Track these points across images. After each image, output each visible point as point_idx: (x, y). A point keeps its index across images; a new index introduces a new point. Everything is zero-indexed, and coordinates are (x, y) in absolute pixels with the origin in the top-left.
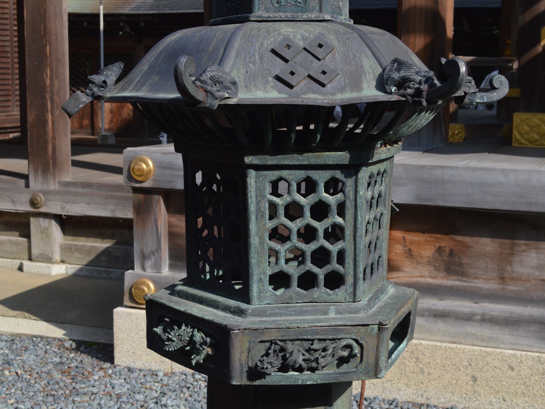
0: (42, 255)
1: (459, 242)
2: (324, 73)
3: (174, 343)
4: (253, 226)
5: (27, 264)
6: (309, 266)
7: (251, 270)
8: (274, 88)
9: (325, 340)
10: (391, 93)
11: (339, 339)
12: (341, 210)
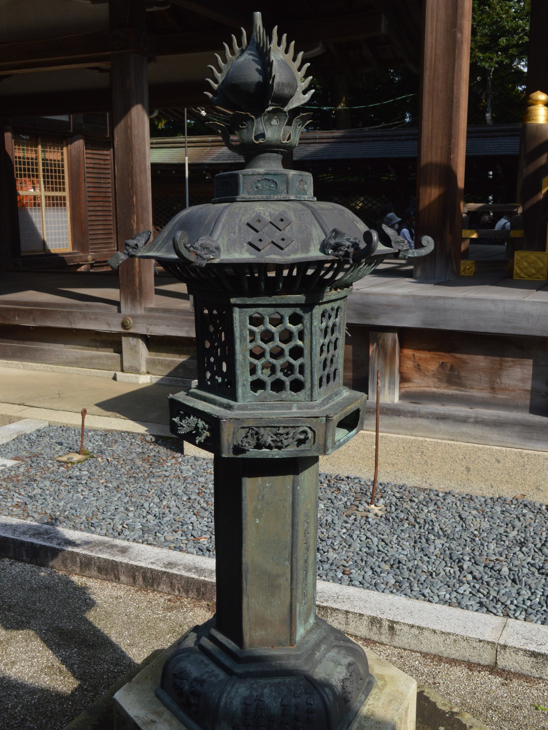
0: (132, 367)
1: (458, 358)
2: (283, 240)
4: (238, 347)
5: (119, 374)
6: (280, 375)
7: (237, 378)
8: (247, 251)
9: (288, 427)
10: (328, 254)
11: (298, 427)
12: (301, 336)
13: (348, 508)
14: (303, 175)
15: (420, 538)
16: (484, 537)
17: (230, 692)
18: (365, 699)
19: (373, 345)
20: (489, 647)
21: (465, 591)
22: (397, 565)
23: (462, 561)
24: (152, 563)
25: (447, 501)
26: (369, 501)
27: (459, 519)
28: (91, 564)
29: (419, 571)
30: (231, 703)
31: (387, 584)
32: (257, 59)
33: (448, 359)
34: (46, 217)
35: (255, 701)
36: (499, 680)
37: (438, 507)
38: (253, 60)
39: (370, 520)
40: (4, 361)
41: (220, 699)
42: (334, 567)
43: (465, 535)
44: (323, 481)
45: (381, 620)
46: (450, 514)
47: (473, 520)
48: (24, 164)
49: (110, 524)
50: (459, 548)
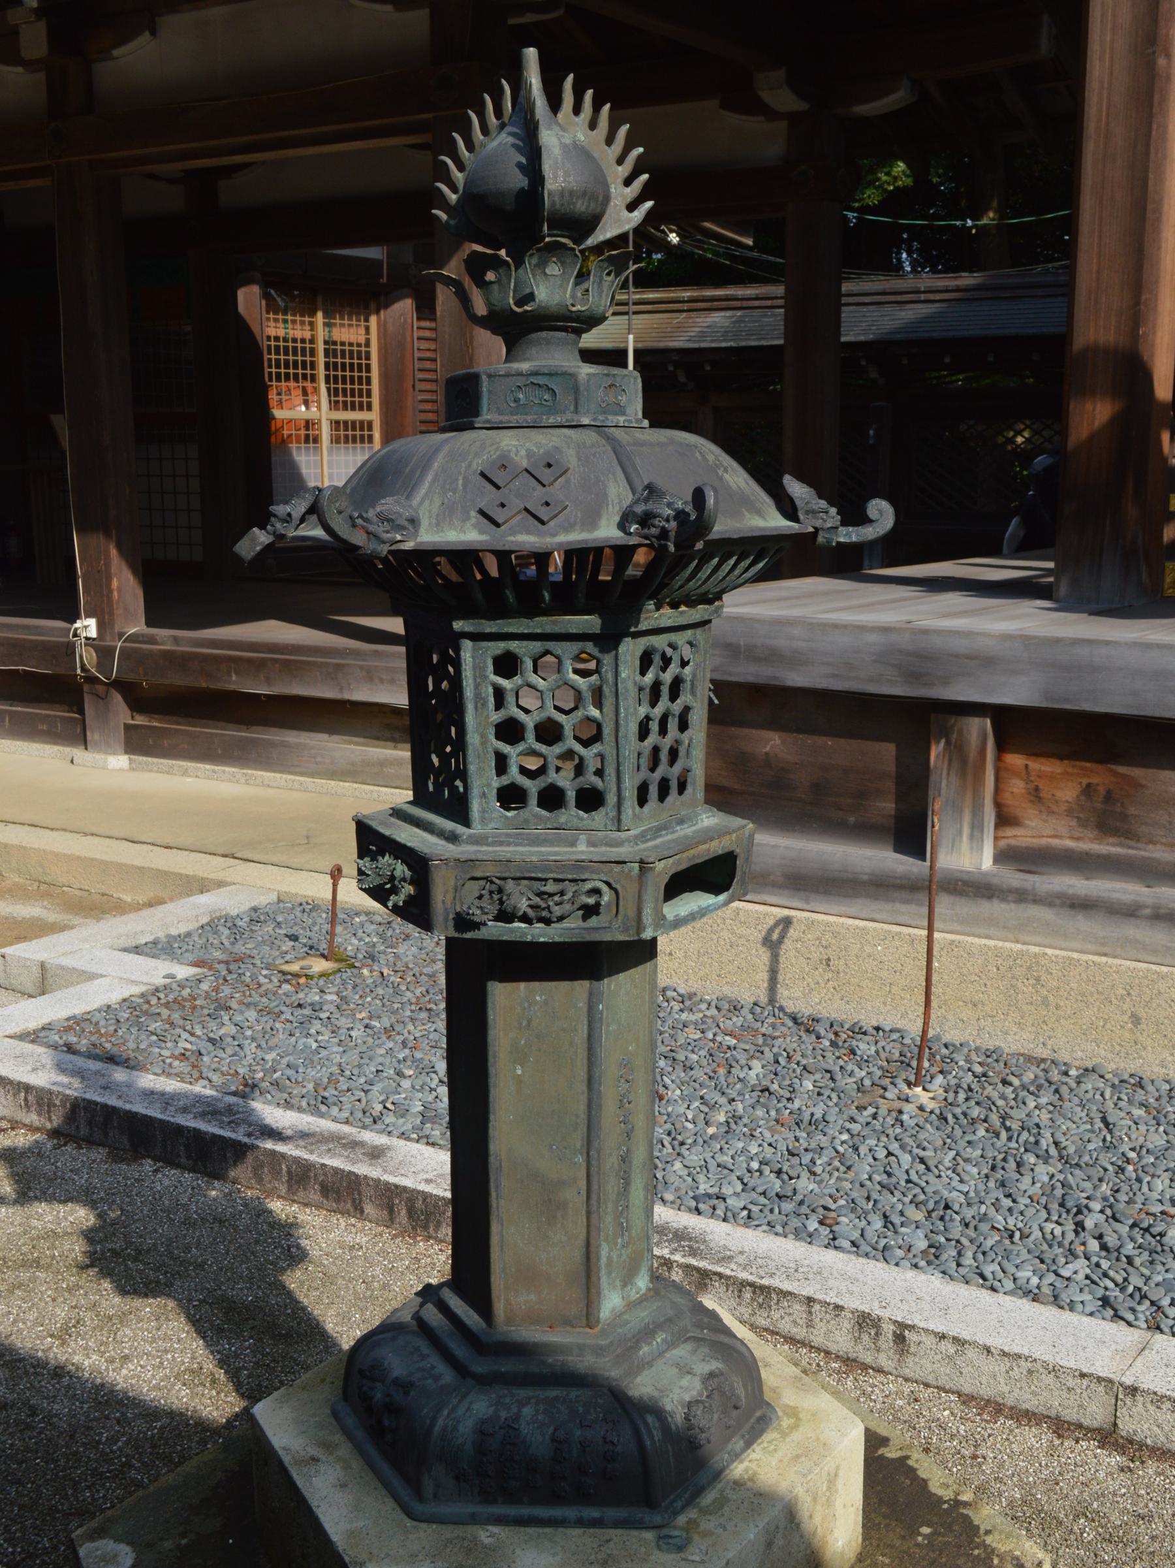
1: (1123, 776)
3: (370, 879)
8: (474, 526)
9: (563, 880)
13: (863, 1092)
14: (614, 375)
15: (1004, 1160)
16: (1147, 1165)
17: (455, 1408)
18: (744, 1450)
19: (938, 743)
20: (1101, 1389)
21: (1075, 1273)
22: (941, 1213)
23: (1085, 1211)
24: (428, 1181)
25: (1083, 1087)
26: (912, 1078)
27: (1102, 1125)
28: (309, 1177)
29: (984, 1227)
30: (455, 1429)
31: (909, 1251)
32: (521, 144)
33: (1100, 777)
34: (330, 467)
35: (501, 1428)
36: (1117, 1459)
37: (1061, 1099)
38: (514, 145)
39: (905, 1117)
40: (208, 767)
41: (434, 1419)
42: (804, 1209)
43: (1105, 1159)
44: (823, 1032)
45: (879, 1320)
46: (1083, 1114)
47: (1130, 1128)
48: (286, 353)
49: (359, 1101)
50: (1088, 1185)
